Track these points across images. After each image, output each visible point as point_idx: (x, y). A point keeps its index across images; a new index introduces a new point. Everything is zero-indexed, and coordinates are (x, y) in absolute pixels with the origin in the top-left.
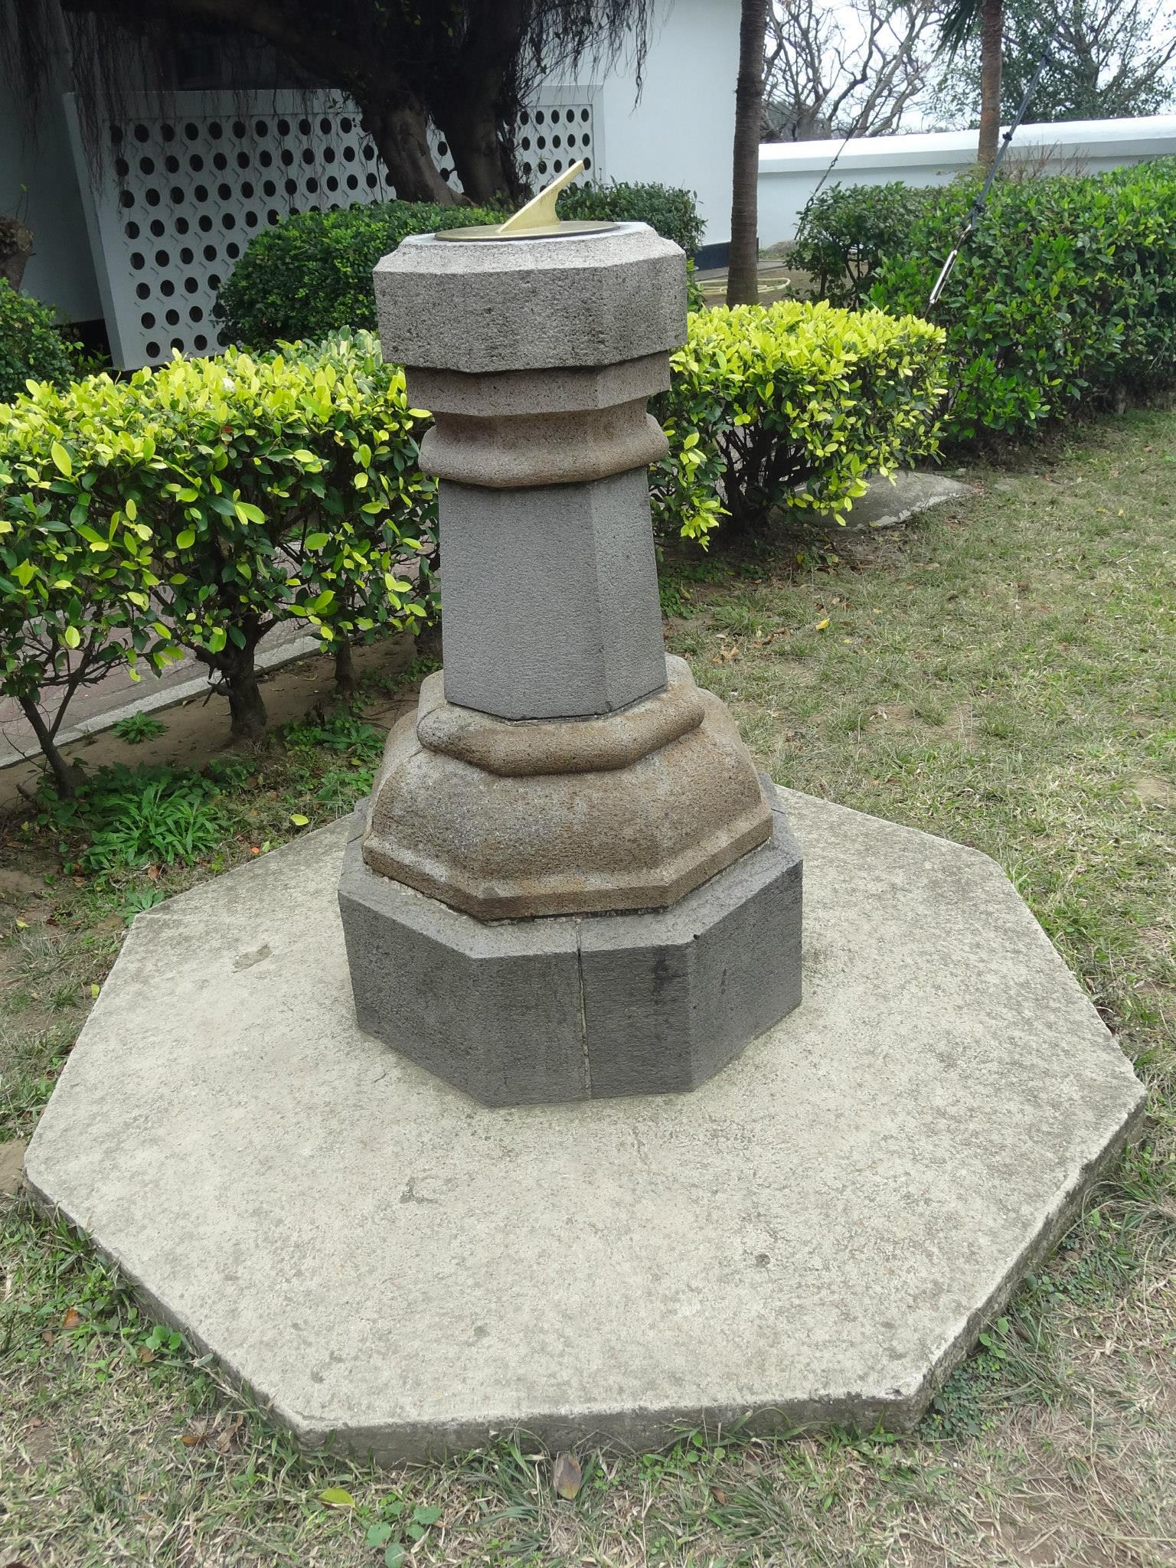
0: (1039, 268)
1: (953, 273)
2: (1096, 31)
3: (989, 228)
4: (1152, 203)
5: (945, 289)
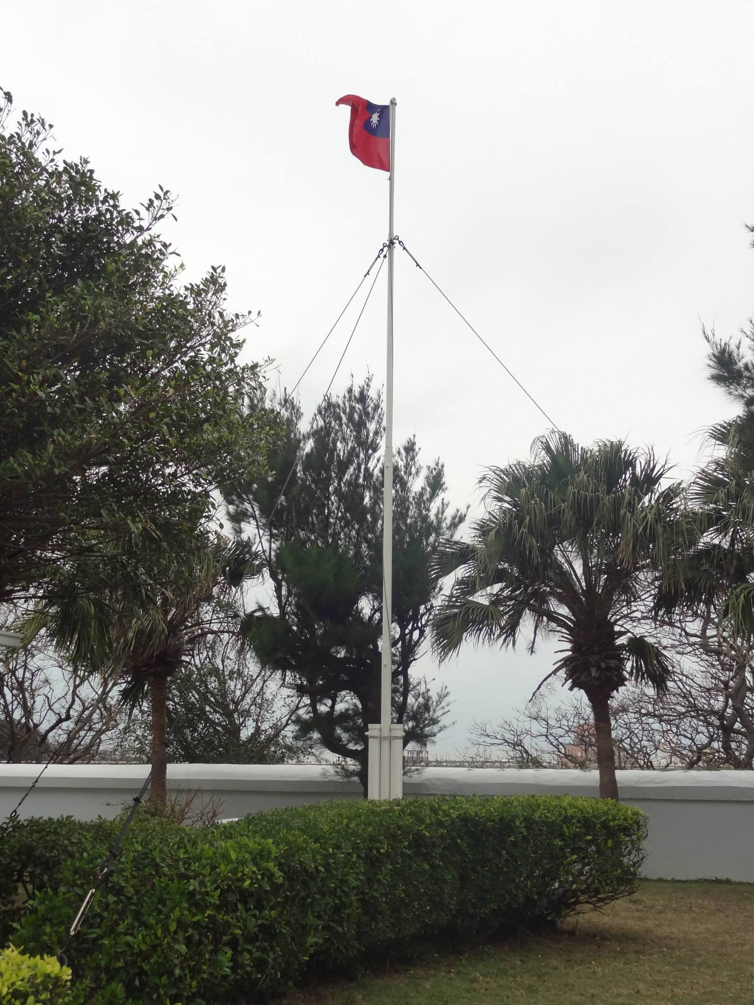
0: (160, 906)
1: (92, 908)
2: (237, 704)
3: (123, 870)
4: (247, 856)
5: (86, 921)
